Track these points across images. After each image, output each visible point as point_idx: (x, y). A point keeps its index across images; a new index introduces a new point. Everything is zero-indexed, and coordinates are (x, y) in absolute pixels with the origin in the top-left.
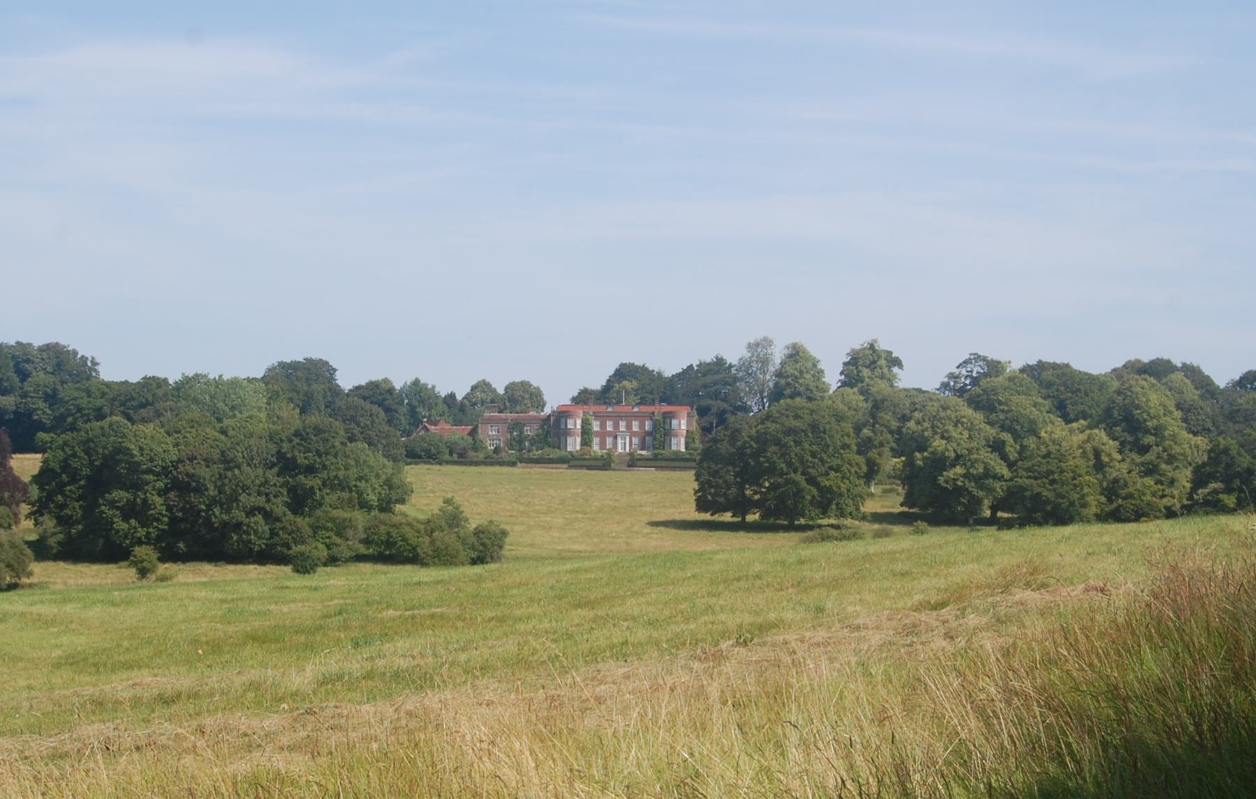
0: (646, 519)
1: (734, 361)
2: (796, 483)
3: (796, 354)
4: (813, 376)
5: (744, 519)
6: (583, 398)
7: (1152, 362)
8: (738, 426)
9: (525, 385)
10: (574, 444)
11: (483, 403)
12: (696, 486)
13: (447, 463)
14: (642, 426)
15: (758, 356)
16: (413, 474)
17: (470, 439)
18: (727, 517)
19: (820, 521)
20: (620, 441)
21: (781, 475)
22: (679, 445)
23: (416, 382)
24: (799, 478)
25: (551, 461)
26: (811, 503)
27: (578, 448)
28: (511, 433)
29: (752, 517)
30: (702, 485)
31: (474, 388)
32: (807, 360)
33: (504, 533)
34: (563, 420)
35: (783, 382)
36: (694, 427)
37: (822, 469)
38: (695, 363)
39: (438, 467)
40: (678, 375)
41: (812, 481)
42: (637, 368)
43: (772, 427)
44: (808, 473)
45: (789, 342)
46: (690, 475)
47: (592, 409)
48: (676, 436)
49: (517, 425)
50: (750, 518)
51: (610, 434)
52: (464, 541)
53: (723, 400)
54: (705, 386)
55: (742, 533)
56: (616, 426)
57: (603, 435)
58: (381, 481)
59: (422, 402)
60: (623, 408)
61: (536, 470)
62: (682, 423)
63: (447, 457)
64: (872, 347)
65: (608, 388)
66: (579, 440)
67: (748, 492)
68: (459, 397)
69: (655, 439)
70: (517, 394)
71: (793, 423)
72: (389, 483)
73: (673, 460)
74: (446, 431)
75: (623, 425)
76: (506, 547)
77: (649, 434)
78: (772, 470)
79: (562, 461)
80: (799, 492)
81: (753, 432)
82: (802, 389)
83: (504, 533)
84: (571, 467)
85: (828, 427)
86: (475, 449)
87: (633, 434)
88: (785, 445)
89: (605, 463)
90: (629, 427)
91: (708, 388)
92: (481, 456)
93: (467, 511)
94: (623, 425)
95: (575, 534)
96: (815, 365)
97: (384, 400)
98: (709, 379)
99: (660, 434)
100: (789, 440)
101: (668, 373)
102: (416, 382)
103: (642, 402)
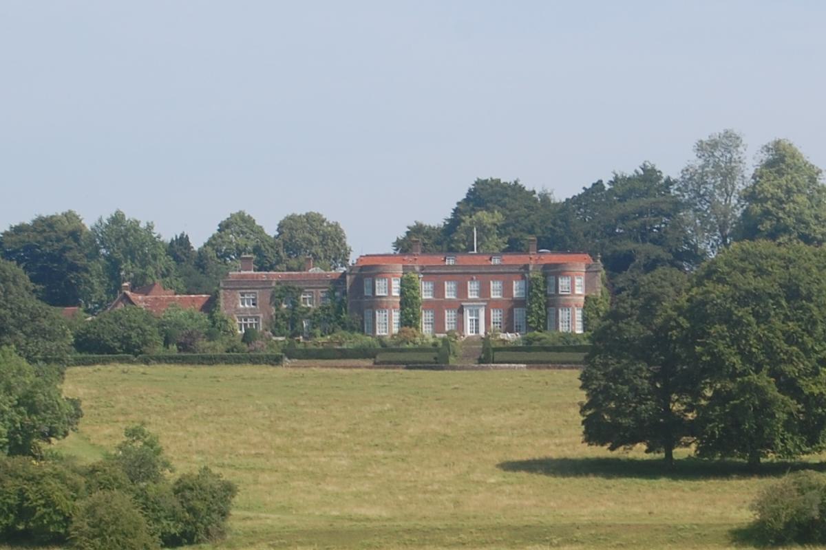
0: (497, 457)
1: (675, 175)
2: (759, 391)
3: (780, 159)
4: (810, 198)
5: (669, 455)
6: (417, 241)
7: (35, 222)
8: (656, 290)
9: (312, 221)
10: (388, 324)
11: (239, 252)
12: (583, 397)
13: (160, 360)
14: (507, 289)
15: (716, 165)
16: (78, 383)
17: (205, 319)
18: (639, 452)
19: (805, 457)
20: (468, 318)
21: (733, 376)
22: (572, 322)
23: (117, 219)
24: (763, 380)
25: (344, 354)
26: (787, 425)
27: (395, 330)
28: (277, 305)
29: (685, 452)
30: (593, 395)
31: (224, 227)
32: (798, 170)
33: (229, 489)
34: (367, 282)
35: (757, 209)
36: (599, 289)
37: (806, 364)
38: (607, 179)
39: (142, 368)
40: (576, 200)
41: (789, 386)
42: (506, 187)
43: (716, 291)
44: (783, 373)
45: (769, 139)
46: (573, 376)
47: (418, 261)
48: (567, 306)
49: (288, 292)
50: (680, 453)
51: (449, 305)
52: (149, 506)
53: (655, 242)
54: (624, 218)
55: (663, 482)
56: (462, 291)
57: (438, 307)
58: (14, 398)
59: (130, 253)
60: (474, 259)
61: (315, 371)
62: (578, 285)
63: (160, 350)
64: (516, 183)
65: (453, 225)
66: (396, 316)
67: (676, 407)
68: (197, 243)
69: (529, 313)
70: (299, 236)
71: (753, 282)
72: (28, 403)
73: (559, 350)
74: (169, 303)
75: (473, 289)
76: (234, 512)
77: (519, 303)
78: (716, 367)
79: (363, 353)
80: (766, 405)
81: (683, 301)
82: (790, 221)
83: (229, 489)
84: (378, 364)
85: (815, 288)
86: (210, 336)
87: (491, 305)
88: (739, 322)
89: (437, 358)
90: (484, 292)
91: (627, 223)
92: (220, 347)
93: (171, 451)
94: (473, 289)
95: (366, 487)
96: (813, 180)
97: (64, 250)
98: (631, 205)
99: (539, 303)
100: (743, 313)
101: (560, 195)
102: (117, 219)
103: (514, 247)
